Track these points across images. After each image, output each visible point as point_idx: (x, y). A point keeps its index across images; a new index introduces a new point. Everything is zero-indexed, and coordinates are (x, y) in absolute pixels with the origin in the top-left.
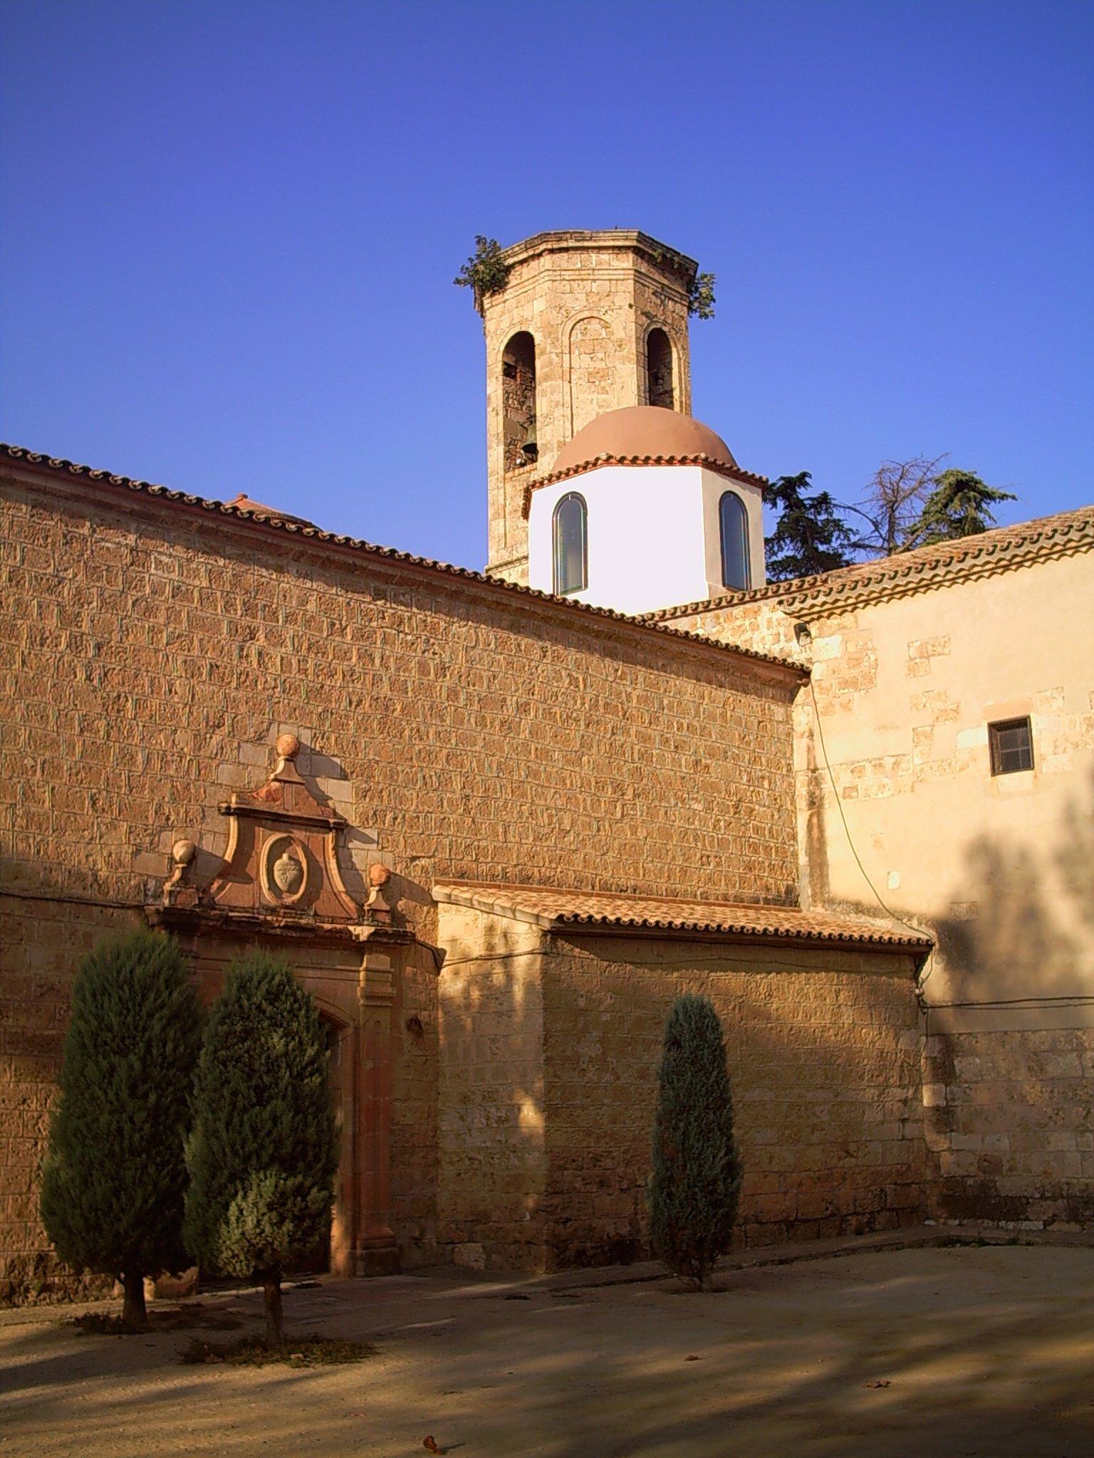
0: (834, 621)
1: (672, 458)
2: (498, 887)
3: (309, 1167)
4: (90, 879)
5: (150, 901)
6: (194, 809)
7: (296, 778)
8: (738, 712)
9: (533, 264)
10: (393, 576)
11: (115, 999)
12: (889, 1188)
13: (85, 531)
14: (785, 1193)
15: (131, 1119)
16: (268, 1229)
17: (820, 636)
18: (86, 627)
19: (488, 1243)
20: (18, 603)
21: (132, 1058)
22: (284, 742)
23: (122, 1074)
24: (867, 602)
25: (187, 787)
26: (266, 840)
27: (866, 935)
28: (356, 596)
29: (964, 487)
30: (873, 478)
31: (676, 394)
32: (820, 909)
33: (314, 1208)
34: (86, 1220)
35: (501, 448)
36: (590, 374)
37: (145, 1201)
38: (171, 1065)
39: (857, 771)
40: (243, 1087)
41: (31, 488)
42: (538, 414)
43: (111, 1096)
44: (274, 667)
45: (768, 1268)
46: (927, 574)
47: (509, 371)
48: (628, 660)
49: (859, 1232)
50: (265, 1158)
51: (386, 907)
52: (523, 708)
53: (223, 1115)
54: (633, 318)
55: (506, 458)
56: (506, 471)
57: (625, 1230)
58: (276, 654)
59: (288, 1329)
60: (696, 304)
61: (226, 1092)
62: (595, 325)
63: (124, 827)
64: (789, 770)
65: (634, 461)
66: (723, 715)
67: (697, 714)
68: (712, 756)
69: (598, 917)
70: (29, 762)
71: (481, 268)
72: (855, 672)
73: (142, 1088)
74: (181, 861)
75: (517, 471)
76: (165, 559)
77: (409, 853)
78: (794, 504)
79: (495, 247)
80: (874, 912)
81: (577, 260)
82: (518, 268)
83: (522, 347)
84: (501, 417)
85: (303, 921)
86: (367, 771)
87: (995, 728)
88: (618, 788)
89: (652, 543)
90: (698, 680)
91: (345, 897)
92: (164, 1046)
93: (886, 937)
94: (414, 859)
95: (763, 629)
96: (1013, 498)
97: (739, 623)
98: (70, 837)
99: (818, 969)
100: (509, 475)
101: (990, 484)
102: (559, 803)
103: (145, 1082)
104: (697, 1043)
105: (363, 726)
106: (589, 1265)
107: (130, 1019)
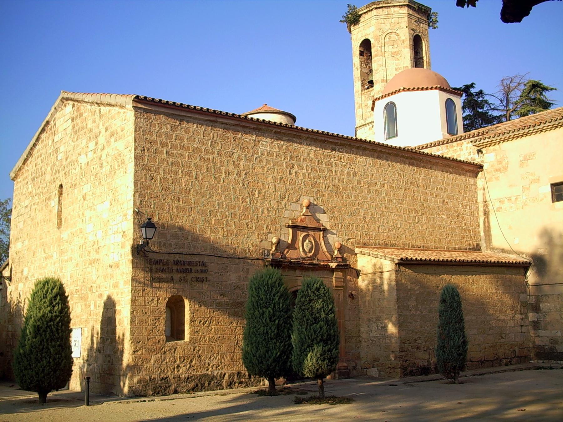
0: (492, 148)
1: (427, 88)
2: (377, 248)
3: (332, 343)
4: (247, 251)
5: (266, 257)
6: (278, 227)
7: (310, 214)
8: (457, 182)
9: (369, 13)
10: (337, 143)
11: (263, 290)
12: (517, 349)
13: (240, 136)
14: (480, 351)
15: (270, 328)
16: (320, 362)
17: (486, 153)
18: (242, 168)
19: (379, 368)
20: (221, 162)
21: (270, 309)
22: (305, 202)
23: (267, 315)
24: (504, 141)
25: (275, 219)
26: (301, 235)
27: (507, 261)
28: (326, 151)
29: (536, 86)
30: (499, 83)
31: (425, 58)
32: (489, 251)
33: (334, 356)
34: (258, 360)
35: (360, 83)
36: (392, 53)
37: (276, 354)
38: (282, 311)
39: (502, 202)
40: (310, 317)
41: (222, 123)
42: (373, 69)
43: (264, 321)
44: (301, 177)
45: (476, 376)
46: (526, 130)
47: (361, 54)
48: (418, 166)
49: (506, 365)
50: (318, 340)
51: (340, 256)
52: (383, 185)
53: (304, 327)
54: (408, 31)
55: (362, 86)
56: (362, 91)
57: (426, 364)
58: (301, 172)
59: (326, 394)
60: (431, 24)
61: (305, 320)
62: (393, 35)
63: (257, 233)
64: (476, 202)
65: (413, 89)
66: (452, 183)
67: (443, 184)
68: (449, 198)
69: (410, 258)
70: (227, 214)
71: (350, 16)
72: (500, 166)
73: (273, 319)
74: (275, 244)
75: (366, 91)
76: (264, 143)
77: (347, 238)
78: (469, 95)
79: (354, 8)
80: (509, 252)
81: (386, 11)
82: (364, 15)
83: (366, 45)
84: (359, 71)
85: (314, 262)
86: (332, 210)
87: (553, 185)
88: (416, 211)
89: (422, 121)
90: (443, 171)
91: (327, 254)
92: (279, 305)
93: (514, 261)
94: (349, 239)
95: (464, 151)
96: (556, 89)
97: (455, 148)
98: (241, 237)
99: (490, 273)
100: (363, 92)
101: (545, 84)
102: (396, 218)
103: (274, 317)
104: (452, 300)
105: (330, 195)
106: (414, 375)
107: (268, 296)
